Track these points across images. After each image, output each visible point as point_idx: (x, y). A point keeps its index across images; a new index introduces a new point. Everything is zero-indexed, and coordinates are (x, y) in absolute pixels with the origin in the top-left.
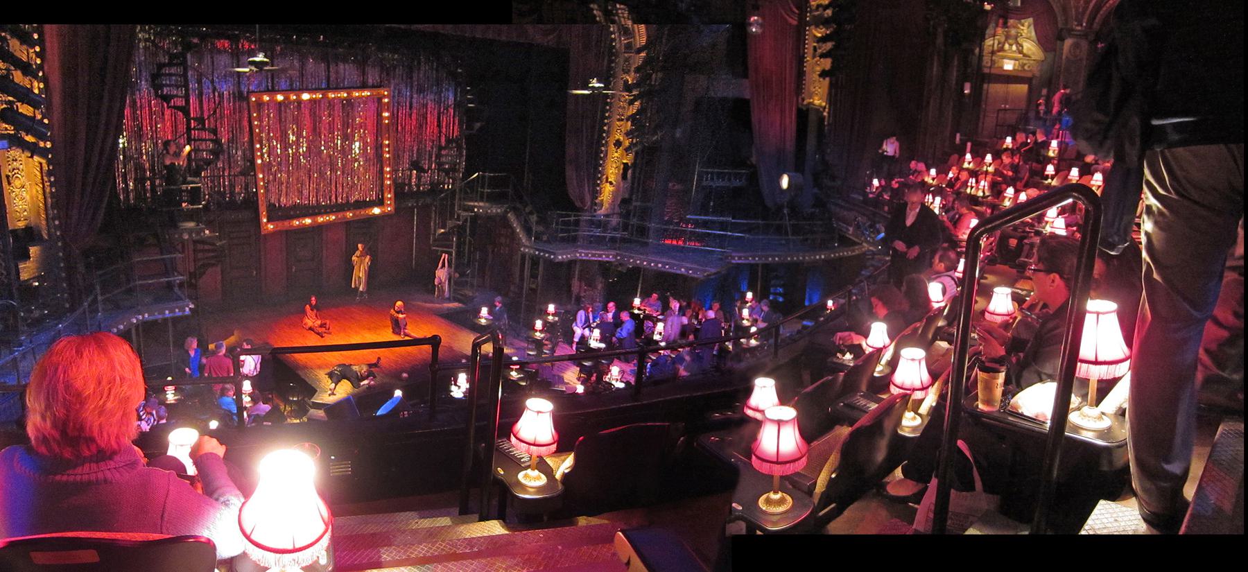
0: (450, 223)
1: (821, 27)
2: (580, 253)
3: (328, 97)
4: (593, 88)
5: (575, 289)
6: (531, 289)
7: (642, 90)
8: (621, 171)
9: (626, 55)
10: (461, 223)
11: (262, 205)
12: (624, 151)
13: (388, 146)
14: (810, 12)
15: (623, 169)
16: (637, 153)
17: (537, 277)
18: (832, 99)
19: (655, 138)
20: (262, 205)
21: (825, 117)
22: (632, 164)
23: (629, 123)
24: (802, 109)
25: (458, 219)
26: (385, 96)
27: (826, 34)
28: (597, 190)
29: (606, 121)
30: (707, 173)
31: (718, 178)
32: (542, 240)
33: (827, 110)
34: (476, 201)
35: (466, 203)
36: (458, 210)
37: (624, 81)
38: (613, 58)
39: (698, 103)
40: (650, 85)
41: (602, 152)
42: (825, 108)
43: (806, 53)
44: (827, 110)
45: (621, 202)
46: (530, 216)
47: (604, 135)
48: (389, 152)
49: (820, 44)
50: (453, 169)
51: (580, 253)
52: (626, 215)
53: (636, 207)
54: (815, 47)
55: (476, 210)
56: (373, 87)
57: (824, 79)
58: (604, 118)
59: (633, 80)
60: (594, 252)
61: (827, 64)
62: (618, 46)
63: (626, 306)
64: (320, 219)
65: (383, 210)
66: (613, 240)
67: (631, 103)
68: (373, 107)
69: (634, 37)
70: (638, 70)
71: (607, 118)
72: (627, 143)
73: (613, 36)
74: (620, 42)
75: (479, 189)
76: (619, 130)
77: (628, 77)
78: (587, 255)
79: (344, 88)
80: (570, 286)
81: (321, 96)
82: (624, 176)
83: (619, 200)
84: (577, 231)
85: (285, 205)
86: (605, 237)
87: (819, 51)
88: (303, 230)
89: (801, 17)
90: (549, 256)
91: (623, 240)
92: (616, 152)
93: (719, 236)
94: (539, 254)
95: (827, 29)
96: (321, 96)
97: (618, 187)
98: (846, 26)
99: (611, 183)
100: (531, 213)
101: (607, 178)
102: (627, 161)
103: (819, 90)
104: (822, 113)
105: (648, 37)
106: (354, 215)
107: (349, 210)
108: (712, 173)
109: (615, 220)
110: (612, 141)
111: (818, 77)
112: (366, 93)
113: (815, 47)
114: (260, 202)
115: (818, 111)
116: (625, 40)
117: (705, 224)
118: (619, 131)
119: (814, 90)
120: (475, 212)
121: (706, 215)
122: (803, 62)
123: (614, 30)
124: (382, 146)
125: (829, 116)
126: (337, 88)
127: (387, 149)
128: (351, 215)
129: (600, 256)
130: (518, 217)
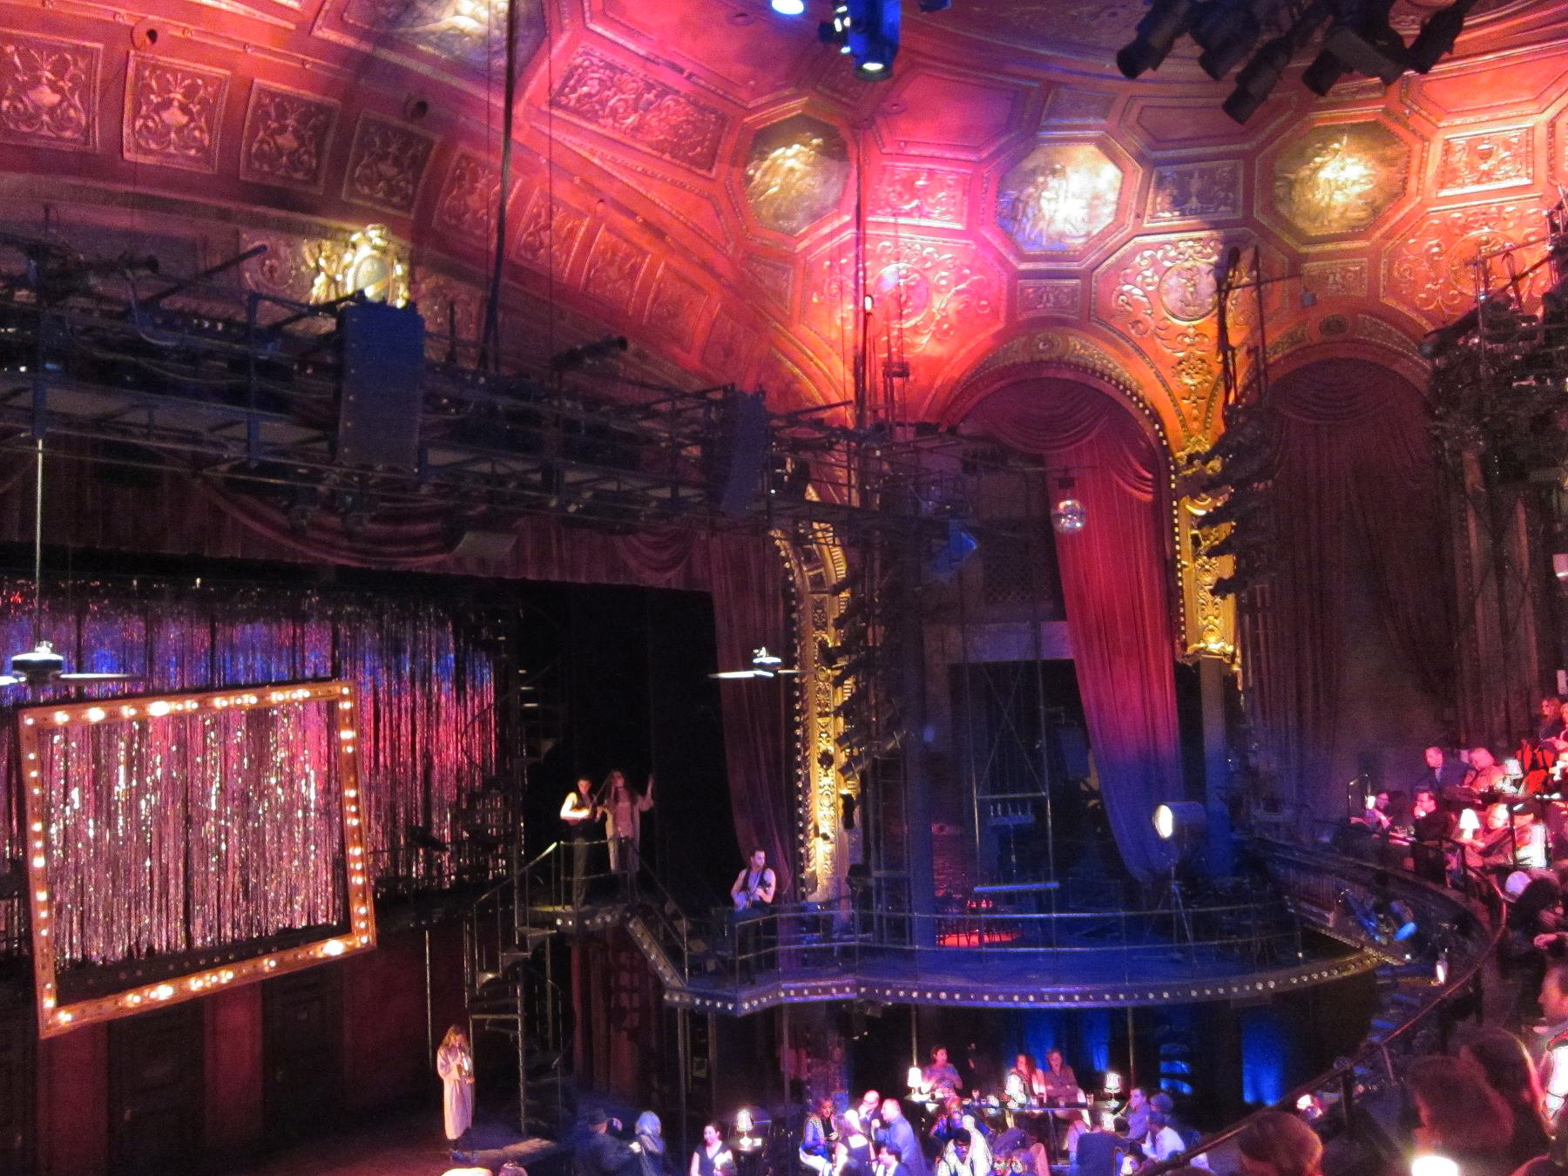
0: (505, 958)
1: (1203, 495)
2: (787, 991)
3: (213, 708)
4: (762, 666)
5: (787, 1069)
6: (696, 1080)
7: (854, 657)
8: (841, 811)
9: (815, 597)
10: (528, 954)
11: (44, 968)
12: (839, 774)
13: (356, 801)
14: (1176, 472)
15: (845, 806)
16: (863, 775)
17: (707, 1052)
18: (1245, 634)
19: (890, 746)
20: (44, 968)
21: (1235, 675)
22: (858, 796)
23: (841, 720)
24: (1185, 665)
25: (522, 946)
26: (343, 698)
27: (1216, 508)
28: (801, 854)
29: (797, 719)
30: (994, 803)
31: (1015, 810)
32: (705, 972)
33: (1238, 660)
34: (558, 904)
35: (538, 909)
36: (520, 925)
37: (820, 643)
38: (794, 603)
39: (955, 671)
40: (866, 648)
41: (799, 777)
42: (1233, 655)
43: (1179, 552)
44: (1238, 660)
45: (850, 873)
46: (676, 923)
47: (799, 745)
48: (357, 814)
49: (1205, 530)
50: (509, 838)
51: (787, 991)
52: (863, 899)
53: (878, 880)
54: (1195, 538)
55: (559, 922)
56: (316, 680)
57: (1223, 598)
58: (792, 713)
59: (835, 642)
60: (813, 984)
61: (1225, 566)
62: (798, 581)
63: (895, 1089)
64: (196, 984)
65: (350, 943)
66: (847, 952)
67: (838, 682)
68: (316, 721)
69: (824, 565)
70: (839, 623)
71: (799, 713)
72: (842, 758)
73: (787, 565)
74: (801, 576)
75: (562, 878)
76: (825, 734)
77: (826, 636)
78: (799, 992)
79: (247, 687)
80: (776, 1063)
81: (195, 706)
82: (848, 822)
83: (847, 868)
84: (773, 943)
85: (104, 959)
86: (831, 950)
87: (1205, 544)
88: (156, 1015)
89: (1160, 483)
90: (724, 1007)
91: (867, 951)
92: (827, 775)
93: (1041, 921)
94: (703, 1003)
95: (1215, 498)
96: (195, 706)
97: (839, 842)
98: (1256, 485)
99: (825, 837)
100: (676, 916)
101: (816, 828)
102: (849, 792)
103: (1217, 622)
104: (1229, 666)
105: (850, 566)
106: (280, 964)
107: (268, 953)
108: (1004, 802)
109: (844, 912)
110: (814, 756)
111: (1209, 596)
112: (302, 693)
113: (1195, 538)
114: (39, 960)
115: (1220, 664)
116: (809, 570)
117: (1010, 898)
118: (824, 735)
119: (1205, 623)
120: (557, 927)
121: (1007, 882)
122: (1176, 570)
123: (788, 555)
124: (342, 802)
125: (1245, 673)
126: (233, 687)
127: (353, 809)
128: (273, 964)
129: (826, 990)
130: (650, 925)
